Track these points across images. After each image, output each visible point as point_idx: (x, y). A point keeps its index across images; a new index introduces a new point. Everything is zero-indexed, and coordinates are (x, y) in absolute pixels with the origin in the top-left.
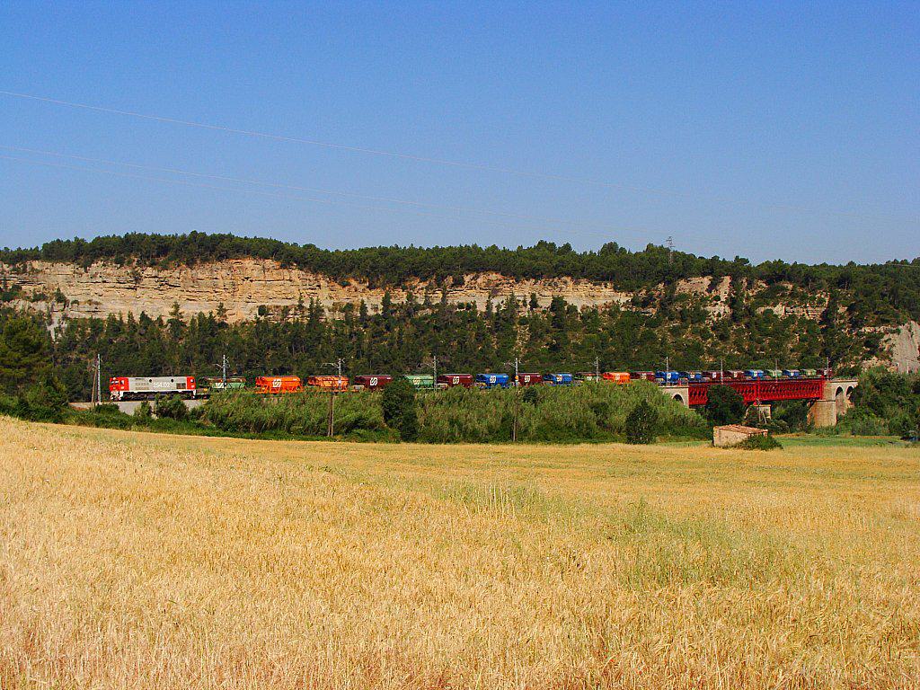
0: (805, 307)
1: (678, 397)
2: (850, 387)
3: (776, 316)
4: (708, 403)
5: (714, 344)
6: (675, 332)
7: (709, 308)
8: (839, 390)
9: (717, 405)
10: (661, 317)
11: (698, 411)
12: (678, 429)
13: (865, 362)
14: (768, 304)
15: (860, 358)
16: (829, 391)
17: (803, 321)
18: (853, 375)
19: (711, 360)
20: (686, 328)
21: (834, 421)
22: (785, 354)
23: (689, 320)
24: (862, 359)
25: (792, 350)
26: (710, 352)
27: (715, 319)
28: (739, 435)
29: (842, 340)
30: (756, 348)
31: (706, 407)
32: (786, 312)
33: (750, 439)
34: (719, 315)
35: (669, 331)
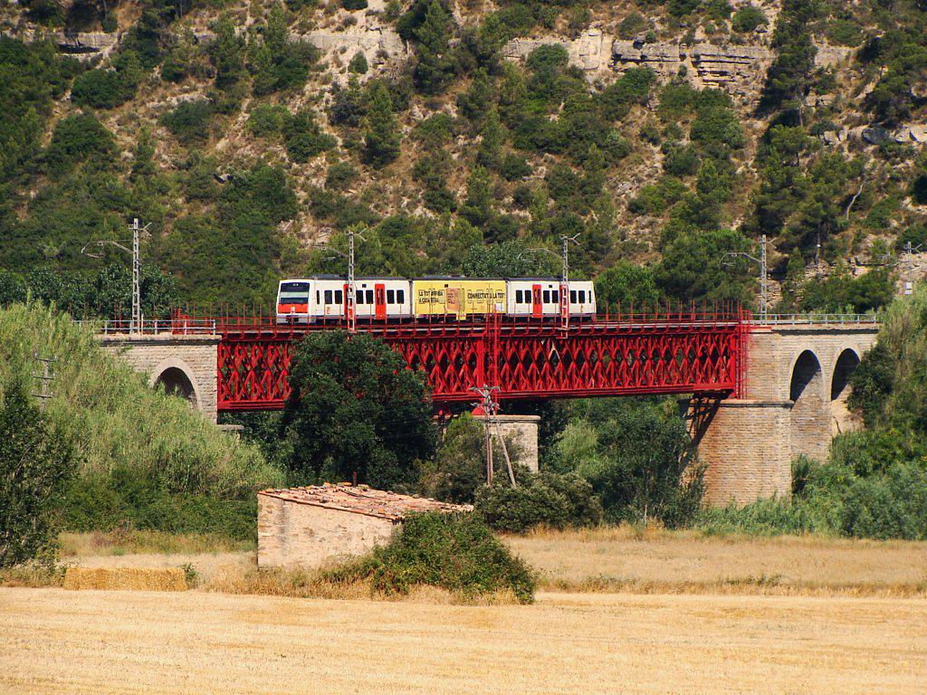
0: (689, 41)
1: (174, 380)
2: (848, 355)
3: (577, 74)
4: (295, 404)
5: (339, 178)
6: (187, 125)
7: (321, 37)
8: (806, 366)
9: (326, 409)
10: (135, 70)
11: (252, 430)
12: (165, 502)
13: (908, 257)
14: (549, 27)
15: (890, 241)
16: (768, 368)
17: (680, 97)
18: (861, 309)
19: (323, 238)
20: (231, 110)
21: (782, 483)
22: (606, 218)
23: (248, 83)
24: (899, 248)
25: (635, 208)
26: (321, 209)
27: (343, 81)
28: (358, 524)
29: (829, 170)
30: (499, 195)
31: (287, 420)
32: (617, 57)
33: (412, 530)
34: (359, 65)
35: (165, 122)
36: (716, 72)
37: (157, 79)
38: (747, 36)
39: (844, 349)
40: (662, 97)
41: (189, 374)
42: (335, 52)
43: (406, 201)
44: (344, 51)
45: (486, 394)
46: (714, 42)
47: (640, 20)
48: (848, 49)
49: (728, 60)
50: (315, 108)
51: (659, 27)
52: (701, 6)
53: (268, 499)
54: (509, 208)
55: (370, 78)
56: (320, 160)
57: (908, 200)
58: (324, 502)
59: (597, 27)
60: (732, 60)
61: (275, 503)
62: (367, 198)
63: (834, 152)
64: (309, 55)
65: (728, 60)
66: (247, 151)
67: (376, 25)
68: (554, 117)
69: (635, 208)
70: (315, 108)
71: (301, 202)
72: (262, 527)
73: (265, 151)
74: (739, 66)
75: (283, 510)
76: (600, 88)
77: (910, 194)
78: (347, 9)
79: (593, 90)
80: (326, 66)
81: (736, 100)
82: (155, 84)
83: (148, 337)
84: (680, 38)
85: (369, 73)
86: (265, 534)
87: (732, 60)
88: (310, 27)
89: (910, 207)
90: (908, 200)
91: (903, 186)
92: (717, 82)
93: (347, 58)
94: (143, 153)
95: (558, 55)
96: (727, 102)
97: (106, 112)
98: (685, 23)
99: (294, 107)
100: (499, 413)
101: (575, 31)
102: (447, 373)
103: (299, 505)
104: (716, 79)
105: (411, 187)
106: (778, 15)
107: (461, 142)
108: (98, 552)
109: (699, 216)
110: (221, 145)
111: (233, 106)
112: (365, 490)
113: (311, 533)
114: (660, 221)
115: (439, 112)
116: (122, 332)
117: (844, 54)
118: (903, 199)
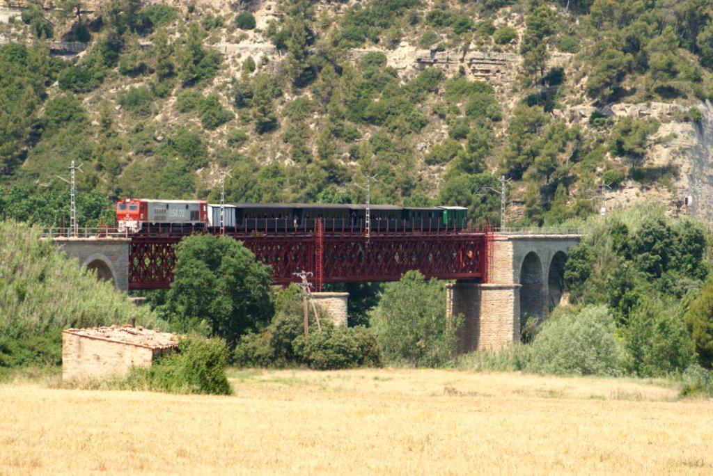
3: (394, 73)
6: (133, 103)
20: (164, 95)
27: (238, 75)
34: (250, 66)
36: (482, 70)
37: (116, 74)
38: (503, 47)
39: (557, 251)
40: (448, 87)
41: (109, 263)
42: (233, 57)
43: (279, 154)
44: (239, 56)
45: (303, 277)
46: (482, 50)
47: (435, 36)
48: (570, 54)
49: (491, 62)
50: (221, 94)
51: (446, 41)
52: (474, 27)
53: (69, 336)
54: (345, 159)
55: (256, 74)
56: (224, 129)
57: (608, 154)
58: (108, 337)
59: (405, 41)
60: (494, 62)
61: (75, 338)
62: (254, 153)
63: (560, 123)
64: (217, 59)
65: (491, 62)
66: (174, 120)
67: (260, 39)
68: (377, 100)
69: (429, 162)
70: (221, 94)
71: (210, 155)
72: (66, 354)
73: (187, 121)
74: (499, 66)
75: (80, 342)
76: (407, 81)
77: (609, 150)
78: (242, 28)
79: (403, 82)
80: (228, 66)
81: (496, 89)
82: (115, 77)
83: (81, 239)
84: (460, 47)
85: (256, 71)
86: (67, 359)
87: (494, 62)
88: (218, 40)
89: (610, 159)
90: (608, 154)
91: (605, 145)
92: (483, 76)
93: (240, 61)
94: (106, 124)
95: (380, 60)
96: (492, 91)
97: (81, 95)
98: (463, 38)
99: (207, 92)
100: (313, 290)
101: (394, 43)
102: (288, 265)
103: (93, 342)
104: (483, 74)
105: (282, 146)
106: (524, 32)
107: (316, 116)
108: (29, 382)
109: (470, 167)
110: (158, 118)
111: (166, 92)
112: (141, 330)
113: (98, 358)
114: (444, 168)
115: (301, 97)
116: (62, 235)
117: (568, 58)
118: (605, 153)
